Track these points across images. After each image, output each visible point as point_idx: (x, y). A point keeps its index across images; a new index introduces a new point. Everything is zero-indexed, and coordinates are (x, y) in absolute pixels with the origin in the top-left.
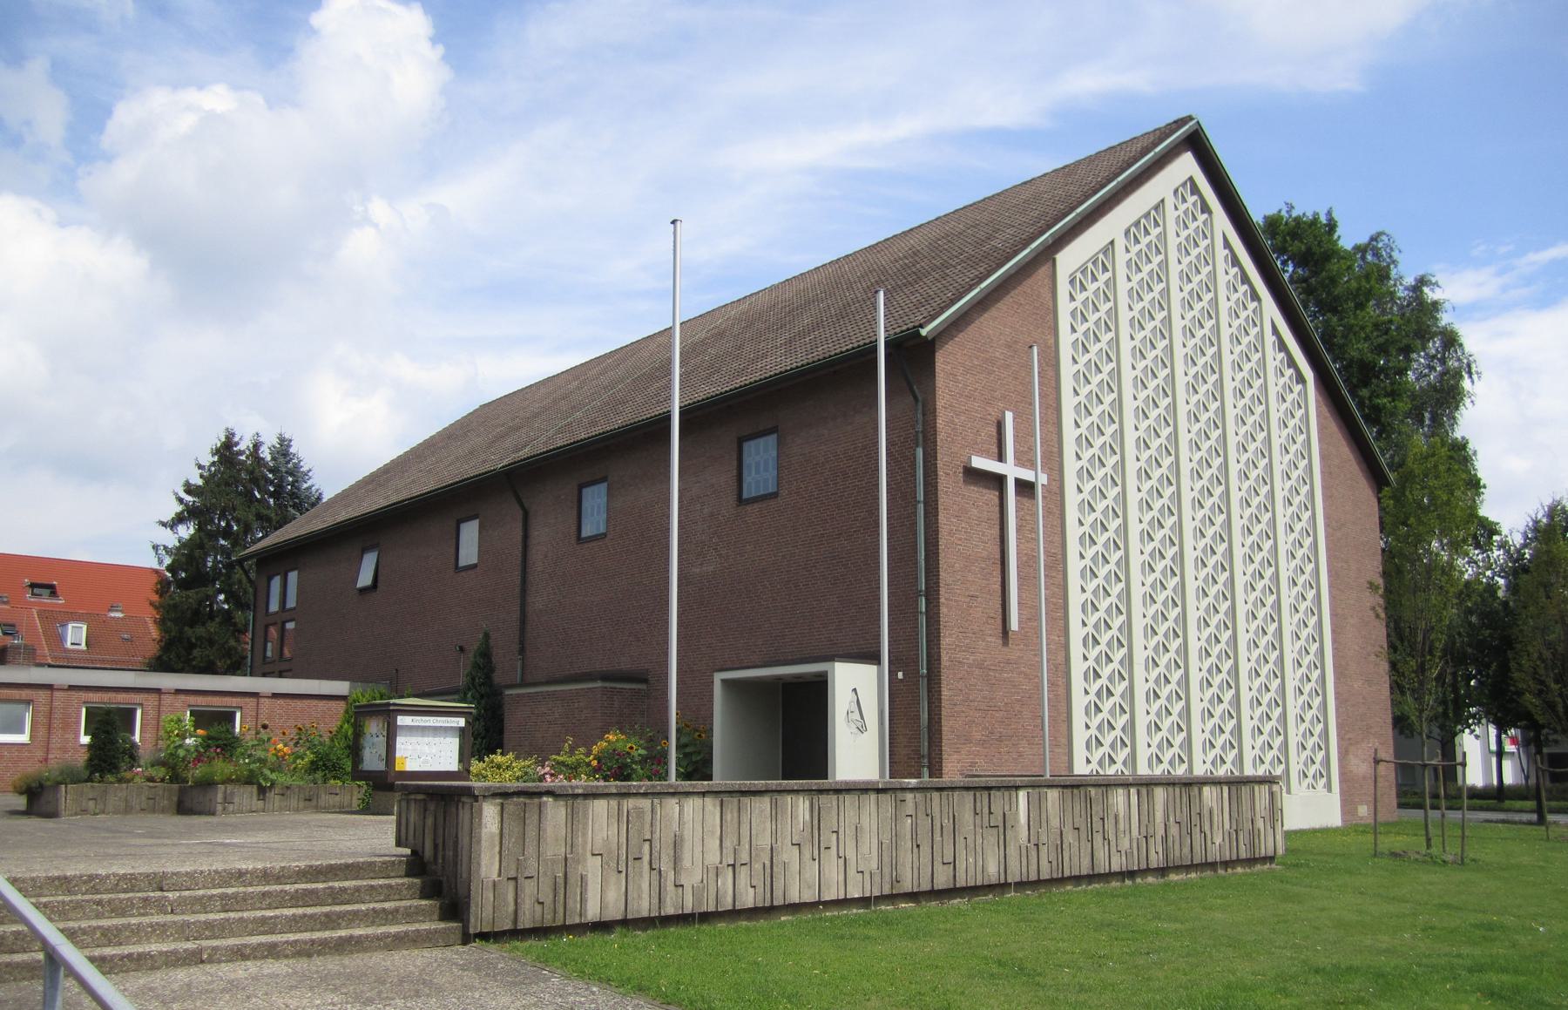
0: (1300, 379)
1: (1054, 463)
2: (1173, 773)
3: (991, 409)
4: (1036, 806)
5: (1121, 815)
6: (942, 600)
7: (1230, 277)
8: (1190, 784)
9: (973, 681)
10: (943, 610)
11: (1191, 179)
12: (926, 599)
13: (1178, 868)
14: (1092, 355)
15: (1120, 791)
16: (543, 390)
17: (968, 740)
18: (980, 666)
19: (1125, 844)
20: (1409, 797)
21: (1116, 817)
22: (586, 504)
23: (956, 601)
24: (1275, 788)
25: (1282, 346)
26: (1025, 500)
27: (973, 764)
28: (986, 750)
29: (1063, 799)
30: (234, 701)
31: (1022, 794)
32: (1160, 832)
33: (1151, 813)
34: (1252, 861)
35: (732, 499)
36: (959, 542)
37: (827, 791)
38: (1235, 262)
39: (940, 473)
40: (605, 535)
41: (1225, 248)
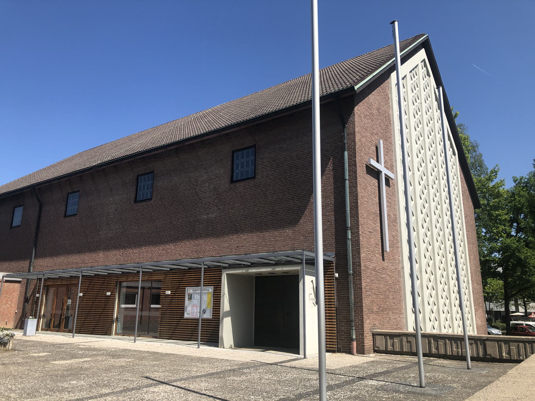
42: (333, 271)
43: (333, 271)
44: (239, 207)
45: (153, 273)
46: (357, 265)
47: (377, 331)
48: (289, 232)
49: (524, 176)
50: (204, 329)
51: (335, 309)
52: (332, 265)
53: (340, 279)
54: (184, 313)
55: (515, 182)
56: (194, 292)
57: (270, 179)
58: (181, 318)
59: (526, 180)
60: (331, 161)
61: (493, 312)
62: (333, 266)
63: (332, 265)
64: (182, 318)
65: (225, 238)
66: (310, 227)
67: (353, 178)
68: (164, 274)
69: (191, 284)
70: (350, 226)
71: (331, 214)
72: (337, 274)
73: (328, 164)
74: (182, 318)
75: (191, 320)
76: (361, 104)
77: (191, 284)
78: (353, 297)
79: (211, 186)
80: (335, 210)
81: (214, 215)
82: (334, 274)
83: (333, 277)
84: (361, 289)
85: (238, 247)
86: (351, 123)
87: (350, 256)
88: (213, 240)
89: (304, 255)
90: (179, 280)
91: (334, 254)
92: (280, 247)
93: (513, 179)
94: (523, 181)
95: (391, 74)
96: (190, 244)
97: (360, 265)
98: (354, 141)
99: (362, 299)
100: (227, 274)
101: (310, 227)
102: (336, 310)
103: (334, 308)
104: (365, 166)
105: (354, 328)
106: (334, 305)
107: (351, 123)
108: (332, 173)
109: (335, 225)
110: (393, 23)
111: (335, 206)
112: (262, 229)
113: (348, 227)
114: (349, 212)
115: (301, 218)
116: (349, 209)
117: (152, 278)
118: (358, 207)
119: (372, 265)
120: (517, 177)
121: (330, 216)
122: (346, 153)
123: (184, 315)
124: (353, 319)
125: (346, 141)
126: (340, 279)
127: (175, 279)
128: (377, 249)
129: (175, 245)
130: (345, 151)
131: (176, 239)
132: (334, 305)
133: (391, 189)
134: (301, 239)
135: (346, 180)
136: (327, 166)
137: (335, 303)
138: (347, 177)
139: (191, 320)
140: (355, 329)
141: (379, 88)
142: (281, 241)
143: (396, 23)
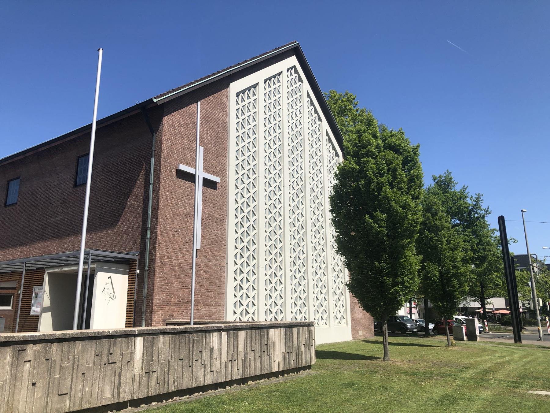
0: (337, 155)
1: (223, 172)
2: (256, 320)
3: (193, 145)
4: (149, 349)
5: (215, 348)
6: (159, 232)
7: (310, 110)
8: (263, 328)
9: (173, 273)
10: (159, 237)
11: (294, 66)
12: (151, 232)
13: (254, 378)
14: (246, 130)
15: (216, 334)
16: (31, 153)
17: (169, 304)
18: (179, 266)
19: (216, 366)
20: (378, 329)
21: (212, 350)
22: (11, 190)
23: (167, 233)
24: (312, 328)
25: (330, 141)
26: (210, 190)
27: (171, 316)
28: (179, 309)
29: (173, 344)
30: (10, 291)
31: (139, 341)
32: (241, 356)
33: (236, 346)
34: (297, 370)
35: (71, 185)
36: (170, 205)
37: (35, 341)
38: (312, 104)
39: (162, 170)
40: (16, 203)
41: (308, 98)
42: (136, 268)
43: (136, 268)
44: (78, 210)
45: (12, 274)
46: (152, 261)
47: (176, 321)
48: (110, 232)
49: (442, 175)
50: (33, 323)
51: (133, 302)
52: (135, 262)
53: (141, 275)
54: (30, 311)
55: (434, 180)
56: (40, 290)
57: (102, 184)
58: (27, 316)
59: (443, 178)
60: (144, 166)
61: (460, 308)
62: (136, 263)
63: (135, 262)
64: (29, 316)
65: (66, 240)
66: (125, 228)
67: (157, 183)
68: (19, 275)
69: (38, 283)
70: (150, 226)
71: (140, 216)
72: (139, 271)
73: (142, 169)
74: (29, 316)
75: (36, 317)
76: (175, 113)
77: (38, 283)
78: (146, 291)
79: (60, 191)
80: (143, 212)
81: (59, 219)
82: (136, 271)
83: (136, 273)
84: (153, 283)
85: (74, 248)
86: (160, 131)
87: (147, 254)
88: (57, 241)
89: (91, 254)
90: (40, 279)
91: (139, 252)
92: (103, 247)
93: (433, 178)
94: (441, 180)
95: (232, 84)
96: (41, 245)
97: (155, 262)
98: (161, 148)
99: (153, 293)
100: (48, 273)
101: (125, 228)
102: (135, 303)
103: (133, 301)
104: (175, 171)
105: (144, 319)
106: (134, 298)
107: (160, 131)
108: (144, 178)
109: (142, 226)
110: (99, 50)
111: (143, 208)
112: (92, 230)
113: (148, 228)
114: (150, 214)
115: (119, 220)
116: (150, 211)
117: (10, 278)
118: (158, 209)
119: (173, 262)
120: (436, 176)
121: (139, 218)
122: (153, 160)
123: (30, 313)
124: (144, 311)
125: (153, 148)
126: (141, 275)
127: (38, 279)
128: (185, 247)
129: (30, 247)
130: (152, 157)
131: (30, 241)
132: (134, 298)
133: (218, 191)
134: (118, 239)
135: (151, 184)
136: (141, 171)
137: (135, 297)
138: (152, 182)
139: (36, 317)
140: (145, 320)
141: (211, 98)
142: (104, 242)
143: (101, 51)
